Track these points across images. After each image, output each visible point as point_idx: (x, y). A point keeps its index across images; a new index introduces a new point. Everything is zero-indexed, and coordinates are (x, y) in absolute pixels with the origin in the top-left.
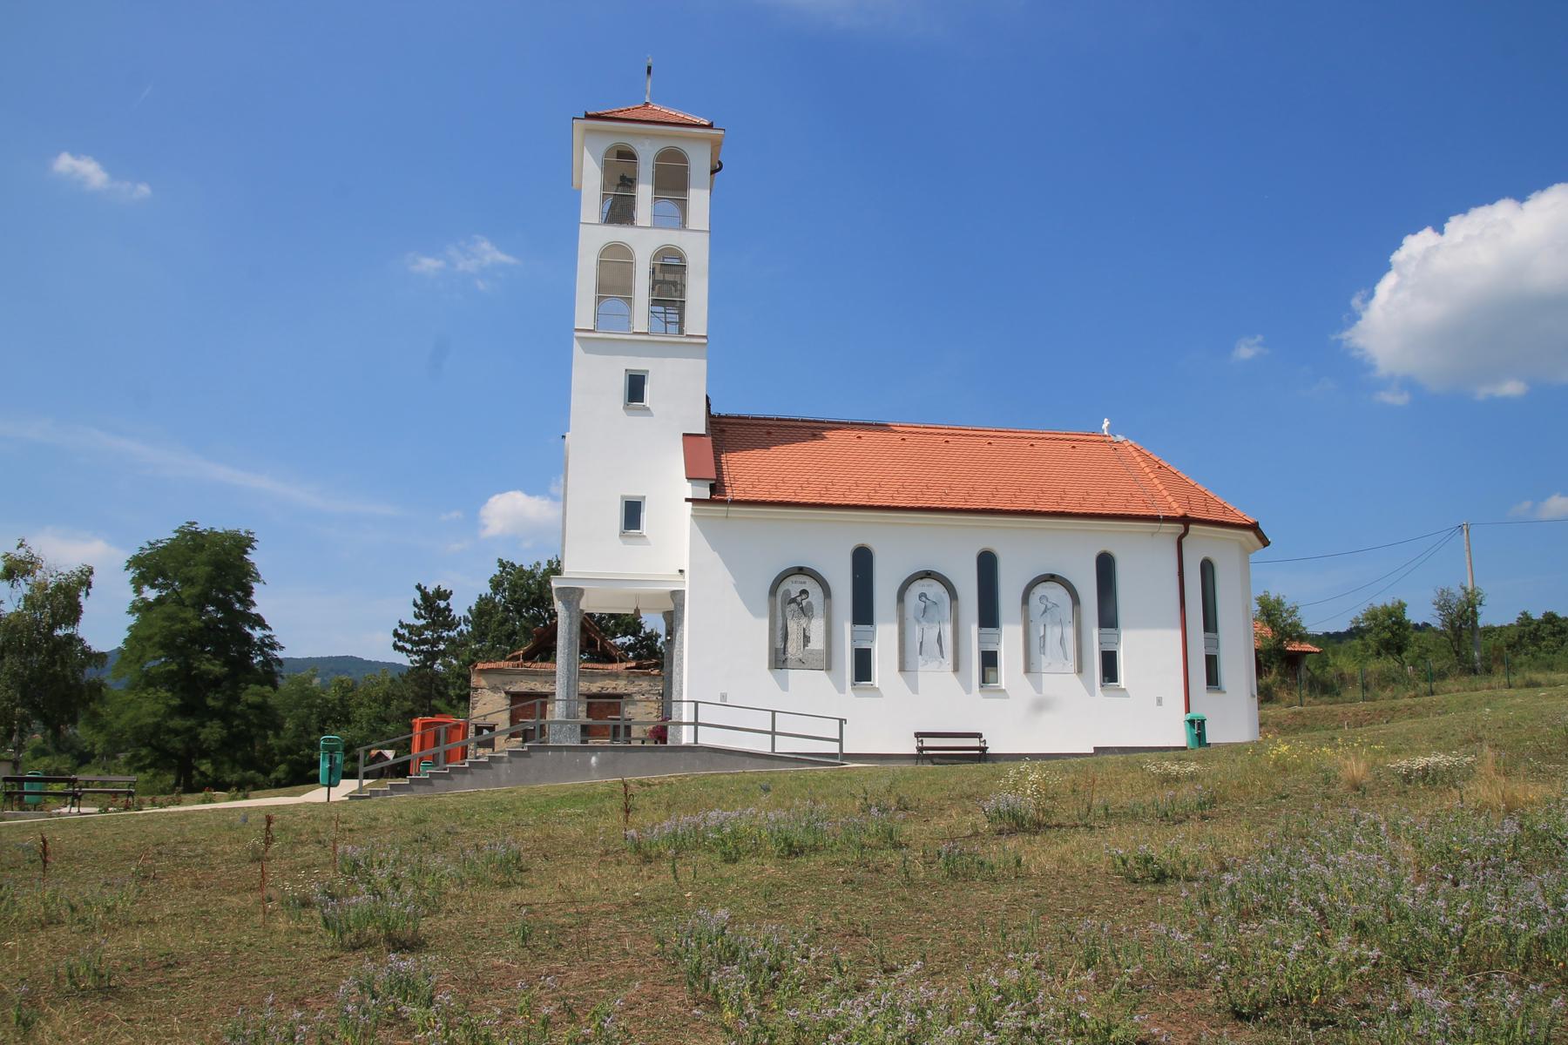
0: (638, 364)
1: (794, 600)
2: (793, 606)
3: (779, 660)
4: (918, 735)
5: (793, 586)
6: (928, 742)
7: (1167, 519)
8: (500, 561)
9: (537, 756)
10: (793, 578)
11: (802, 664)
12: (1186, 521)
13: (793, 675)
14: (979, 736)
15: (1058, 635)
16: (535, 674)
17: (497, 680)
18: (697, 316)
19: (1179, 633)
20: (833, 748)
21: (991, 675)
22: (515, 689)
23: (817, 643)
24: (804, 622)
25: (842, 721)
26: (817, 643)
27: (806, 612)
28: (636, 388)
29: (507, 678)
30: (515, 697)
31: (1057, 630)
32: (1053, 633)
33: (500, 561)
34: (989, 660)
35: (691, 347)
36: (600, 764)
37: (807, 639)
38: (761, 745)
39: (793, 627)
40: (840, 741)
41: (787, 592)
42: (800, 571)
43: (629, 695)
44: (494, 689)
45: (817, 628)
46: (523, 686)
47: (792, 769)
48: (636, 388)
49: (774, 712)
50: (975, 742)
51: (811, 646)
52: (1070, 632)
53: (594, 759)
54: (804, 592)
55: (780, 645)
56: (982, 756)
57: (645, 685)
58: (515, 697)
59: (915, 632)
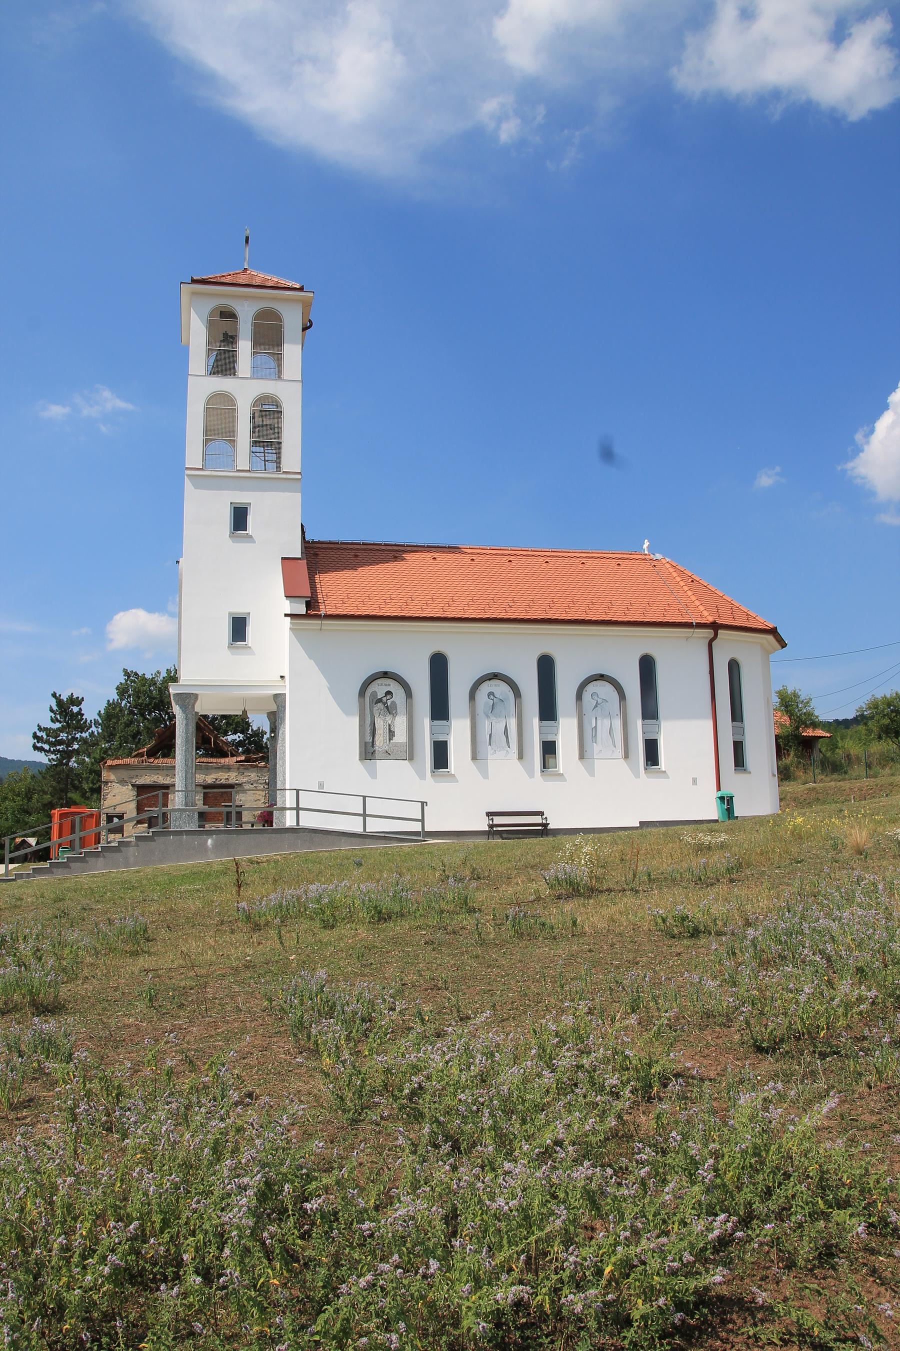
0: (241, 498)
1: (380, 700)
2: (380, 705)
3: (368, 752)
4: (489, 814)
5: (379, 688)
6: (498, 820)
7: (700, 626)
8: (125, 671)
9: (160, 840)
10: (379, 681)
11: (388, 755)
12: (715, 627)
13: (381, 765)
14: (541, 814)
15: (607, 726)
16: (158, 768)
17: (124, 774)
18: (292, 455)
19: (710, 723)
20: (416, 827)
21: (551, 761)
22: (140, 781)
23: (401, 736)
24: (389, 719)
25: (423, 804)
26: (401, 736)
27: (390, 710)
28: (240, 518)
29: (133, 773)
30: (141, 789)
31: (607, 722)
32: (603, 725)
33: (125, 671)
34: (549, 748)
35: (286, 482)
36: (216, 845)
37: (391, 734)
38: (354, 825)
39: (380, 723)
40: (422, 821)
41: (374, 694)
42: (385, 675)
43: (240, 785)
44: (122, 782)
45: (400, 723)
46: (147, 779)
47: (381, 845)
48: (240, 518)
49: (364, 797)
50: (537, 819)
51: (396, 739)
52: (618, 724)
53: (210, 842)
54: (389, 693)
55: (369, 739)
56: (544, 831)
57: (253, 775)
58: (141, 789)
59: (485, 726)
